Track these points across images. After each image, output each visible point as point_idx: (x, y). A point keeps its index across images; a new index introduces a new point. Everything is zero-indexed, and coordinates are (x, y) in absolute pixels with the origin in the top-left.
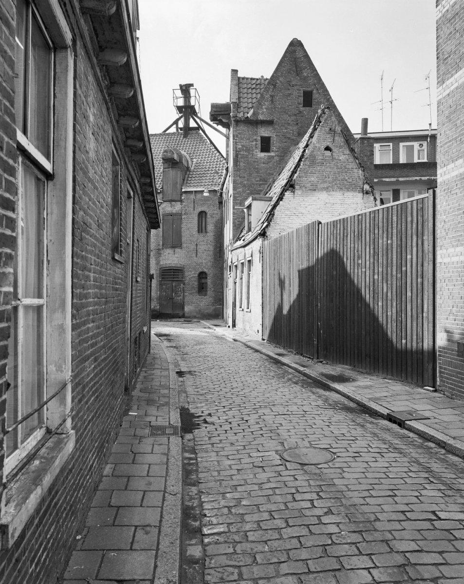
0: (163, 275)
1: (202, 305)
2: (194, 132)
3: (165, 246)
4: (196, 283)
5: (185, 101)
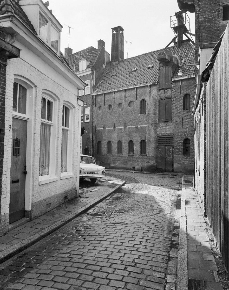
1: (186, 163)
2: (186, 43)
3: (160, 121)
4: (182, 147)
5: (179, 23)
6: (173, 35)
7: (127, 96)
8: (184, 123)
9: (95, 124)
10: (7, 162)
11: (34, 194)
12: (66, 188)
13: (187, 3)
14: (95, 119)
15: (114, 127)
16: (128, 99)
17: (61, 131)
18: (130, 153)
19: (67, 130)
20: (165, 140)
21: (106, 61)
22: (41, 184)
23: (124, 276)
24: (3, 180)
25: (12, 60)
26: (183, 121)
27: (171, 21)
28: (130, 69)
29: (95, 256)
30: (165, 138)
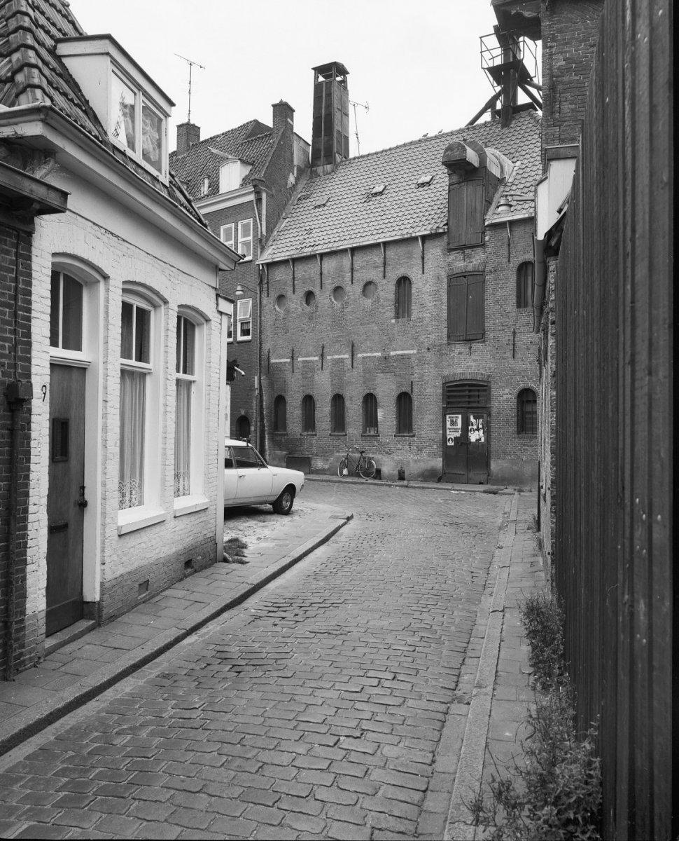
0: (449, 397)
6: (487, 89)
7: (356, 266)
8: (519, 344)
9: (266, 346)
10: (38, 480)
11: (107, 560)
12: (188, 540)
13: (519, 15)
14: (268, 333)
15: (322, 355)
16: (362, 276)
17: (173, 387)
18: (368, 429)
19: (190, 383)
20: (467, 393)
21: (301, 150)
22: (123, 532)
23: (332, 761)
24: (30, 527)
25: (46, 217)
26: (516, 339)
27: (484, 49)
28: (368, 187)
29: (266, 715)
30: (467, 388)
